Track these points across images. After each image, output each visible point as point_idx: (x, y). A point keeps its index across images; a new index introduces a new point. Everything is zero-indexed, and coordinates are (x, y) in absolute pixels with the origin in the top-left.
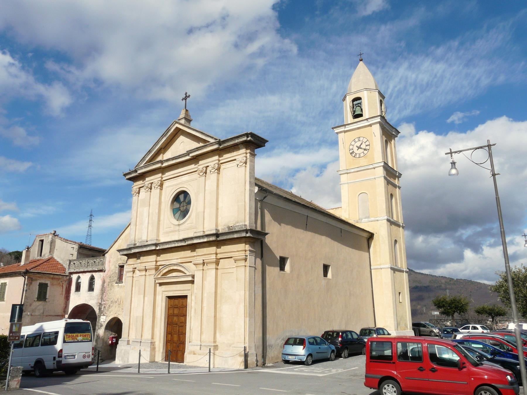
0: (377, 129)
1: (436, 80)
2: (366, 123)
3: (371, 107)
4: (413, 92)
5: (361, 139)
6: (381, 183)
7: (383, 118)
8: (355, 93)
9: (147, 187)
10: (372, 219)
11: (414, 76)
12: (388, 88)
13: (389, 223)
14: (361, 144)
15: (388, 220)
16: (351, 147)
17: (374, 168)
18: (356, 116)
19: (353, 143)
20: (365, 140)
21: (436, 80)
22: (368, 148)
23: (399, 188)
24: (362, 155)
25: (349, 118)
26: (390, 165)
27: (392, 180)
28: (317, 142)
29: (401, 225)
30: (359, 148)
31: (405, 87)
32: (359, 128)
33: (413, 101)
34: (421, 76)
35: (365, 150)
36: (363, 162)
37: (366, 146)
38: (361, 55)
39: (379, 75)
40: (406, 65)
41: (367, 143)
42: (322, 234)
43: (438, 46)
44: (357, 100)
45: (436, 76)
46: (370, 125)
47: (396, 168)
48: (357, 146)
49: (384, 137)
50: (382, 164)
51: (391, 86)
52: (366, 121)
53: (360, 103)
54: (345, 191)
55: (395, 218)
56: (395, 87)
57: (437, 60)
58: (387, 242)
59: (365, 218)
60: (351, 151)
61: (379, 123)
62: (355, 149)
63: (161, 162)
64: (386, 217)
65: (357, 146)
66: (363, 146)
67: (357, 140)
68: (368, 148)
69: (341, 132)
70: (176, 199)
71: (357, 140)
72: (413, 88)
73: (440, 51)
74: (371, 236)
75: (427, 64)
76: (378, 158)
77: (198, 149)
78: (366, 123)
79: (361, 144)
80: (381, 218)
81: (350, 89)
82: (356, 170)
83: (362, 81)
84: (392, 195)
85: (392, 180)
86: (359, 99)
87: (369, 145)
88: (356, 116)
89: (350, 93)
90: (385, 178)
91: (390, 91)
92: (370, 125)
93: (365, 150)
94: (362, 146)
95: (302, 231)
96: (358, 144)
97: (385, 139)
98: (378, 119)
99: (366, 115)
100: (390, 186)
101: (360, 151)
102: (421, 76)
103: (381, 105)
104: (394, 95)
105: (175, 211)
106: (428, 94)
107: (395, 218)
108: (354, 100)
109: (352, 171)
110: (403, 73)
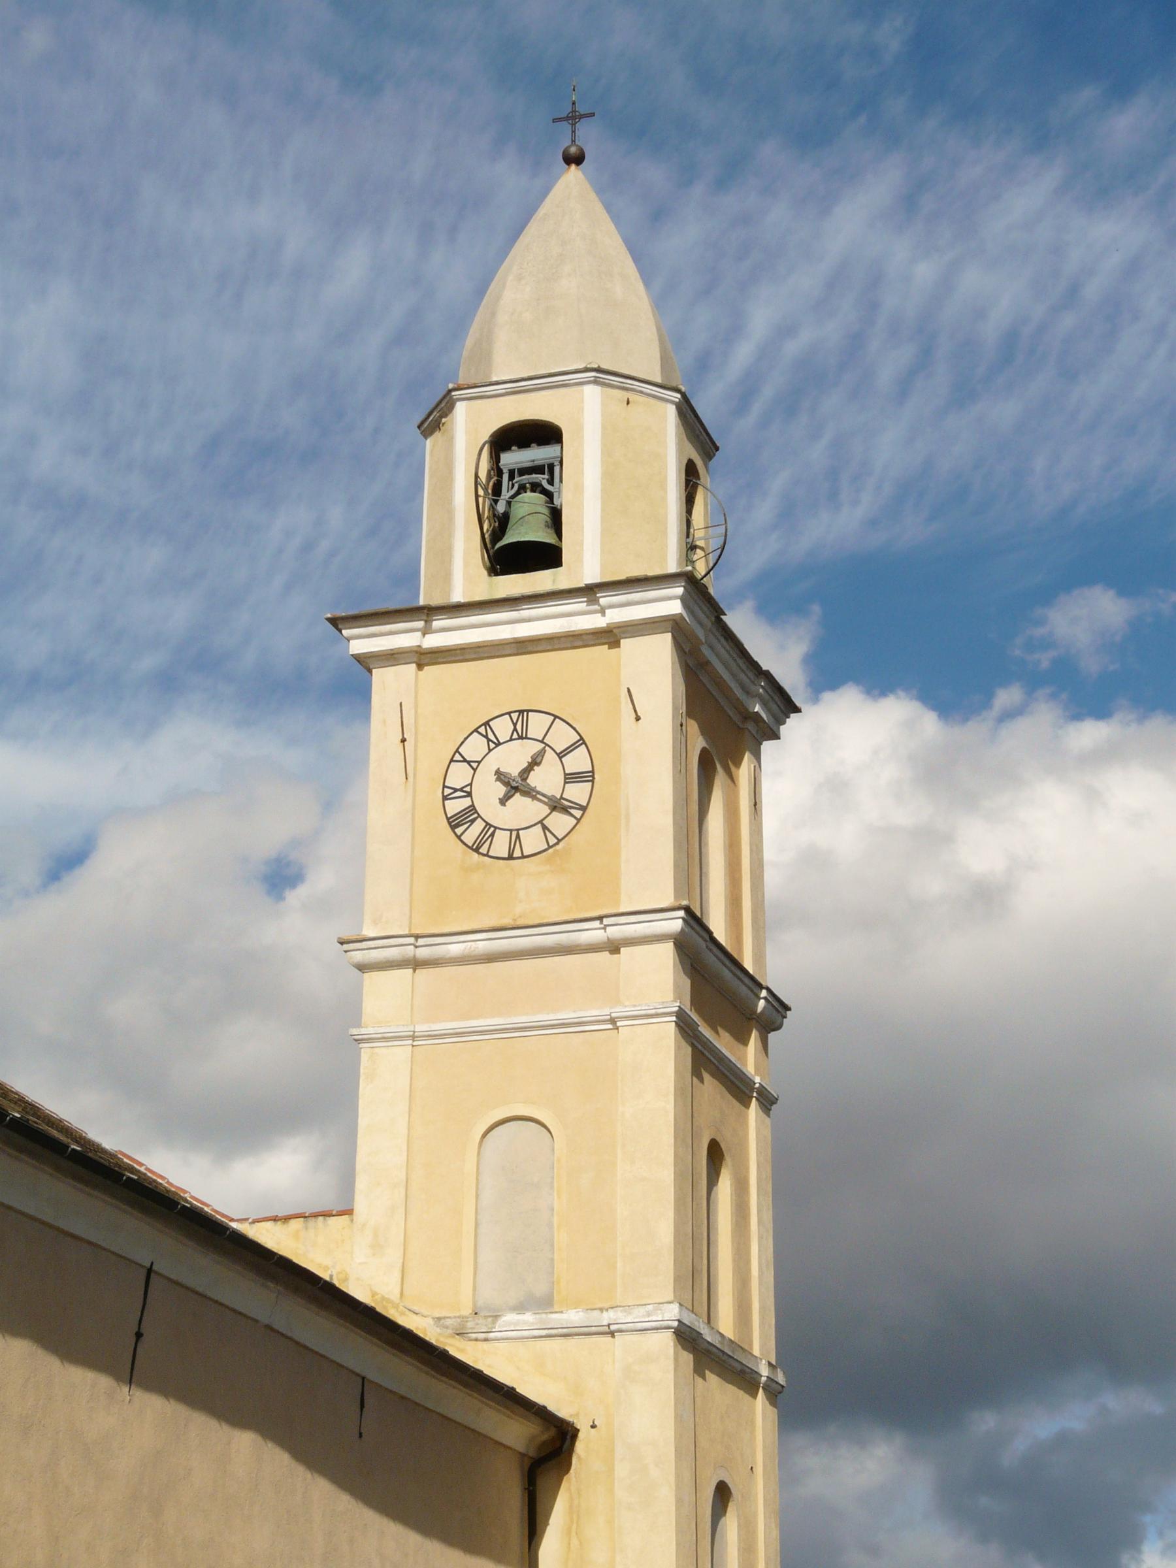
0: (652, 668)
1: (1068, 321)
2: (581, 618)
3: (620, 499)
4: (903, 388)
5: (537, 725)
6: (656, 1053)
7: (696, 589)
8: (519, 386)
10: (574, 1317)
11: (925, 272)
12: (735, 331)
13: (688, 1358)
14: (535, 762)
15: (686, 1337)
16: (459, 776)
17: (614, 947)
18: (509, 558)
19: (475, 747)
20: (562, 737)
21: (1068, 321)
22: (577, 793)
23: (767, 1102)
24: (532, 841)
25: (463, 571)
26: (720, 935)
27: (723, 1043)
28: (150, 662)
29: (764, 1371)
30: (515, 787)
31: (855, 342)
32: (523, 646)
33: (890, 448)
34: (973, 280)
35: (558, 805)
36: (534, 891)
37: (570, 778)
39: (685, 237)
40: (881, 185)
41: (578, 761)
42: (235, 1415)
43: (1121, 90)
44: (524, 444)
45: (1074, 291)
46: (610, 637)
47: (759, 957)
48: (500, 776)
49: (693, 727)
50: (675, 924)
51: (760, 320)
52: (579, 604)
53: (549, 469)
54: (385, 1089)
55: (726, 1324)
56: (785, 330)
57: (1099, 187)
58: (666, 1496)
59: (520, 1308)
60: (456, 806)
61: (674, 625)
62: (487, 793)
64: (672, 1313)
65: (500, 776)
66: (547, 779)
67: (503, 728)
68: (577, 793)
69: (392, 657)
71: (503, 728)
72: (905, 354)
73: (1126, 126)
74: (554, 1444)
75: (1027, 201)
76: (647, 879)
78: (581, 618)
79: (535, 762)
80: (637, 1316)
81: (484, 355)
82: (482, 944)
83: (569, 305)
84: (715, 1154)
85: (723, 1043)
86: (547, 434)
87: (588, 777)
88: (509, 558)
89: (482, 388)
90: (685, 1026)
91: (743, 354)
92: (610, 637)
93: (558, 805)
94: (536, 779)
95: (104, 1382)
96: (513, 758)
97: (698, 743)
98: (669, 603)
99: (586, 556)
100: (710, 1086)
101: (523, 810)
102: (973, 280)
103: (690, 501)
104: (768, 392)
106: (1004, 412)
107: (726, 1324)
108: (510, 437)
109: (455, 948)
110: (848, 233)
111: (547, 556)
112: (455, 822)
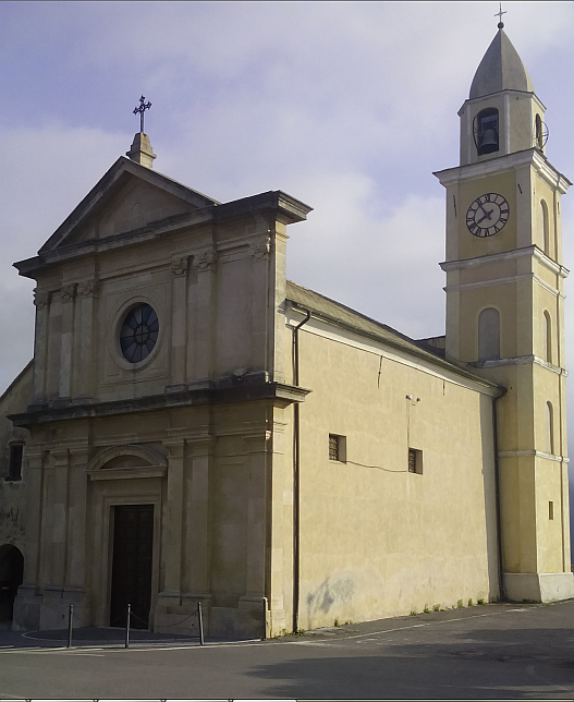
9: (67, 294)
38: (501, 14)
63: (96, 242)
70: (127, 318)
77: (171, 220)
86: (494, 112)
87: (507, 211)
105: (124, 344)
108: (482, 115)
111: (495, 148)
112: (469, 228)
